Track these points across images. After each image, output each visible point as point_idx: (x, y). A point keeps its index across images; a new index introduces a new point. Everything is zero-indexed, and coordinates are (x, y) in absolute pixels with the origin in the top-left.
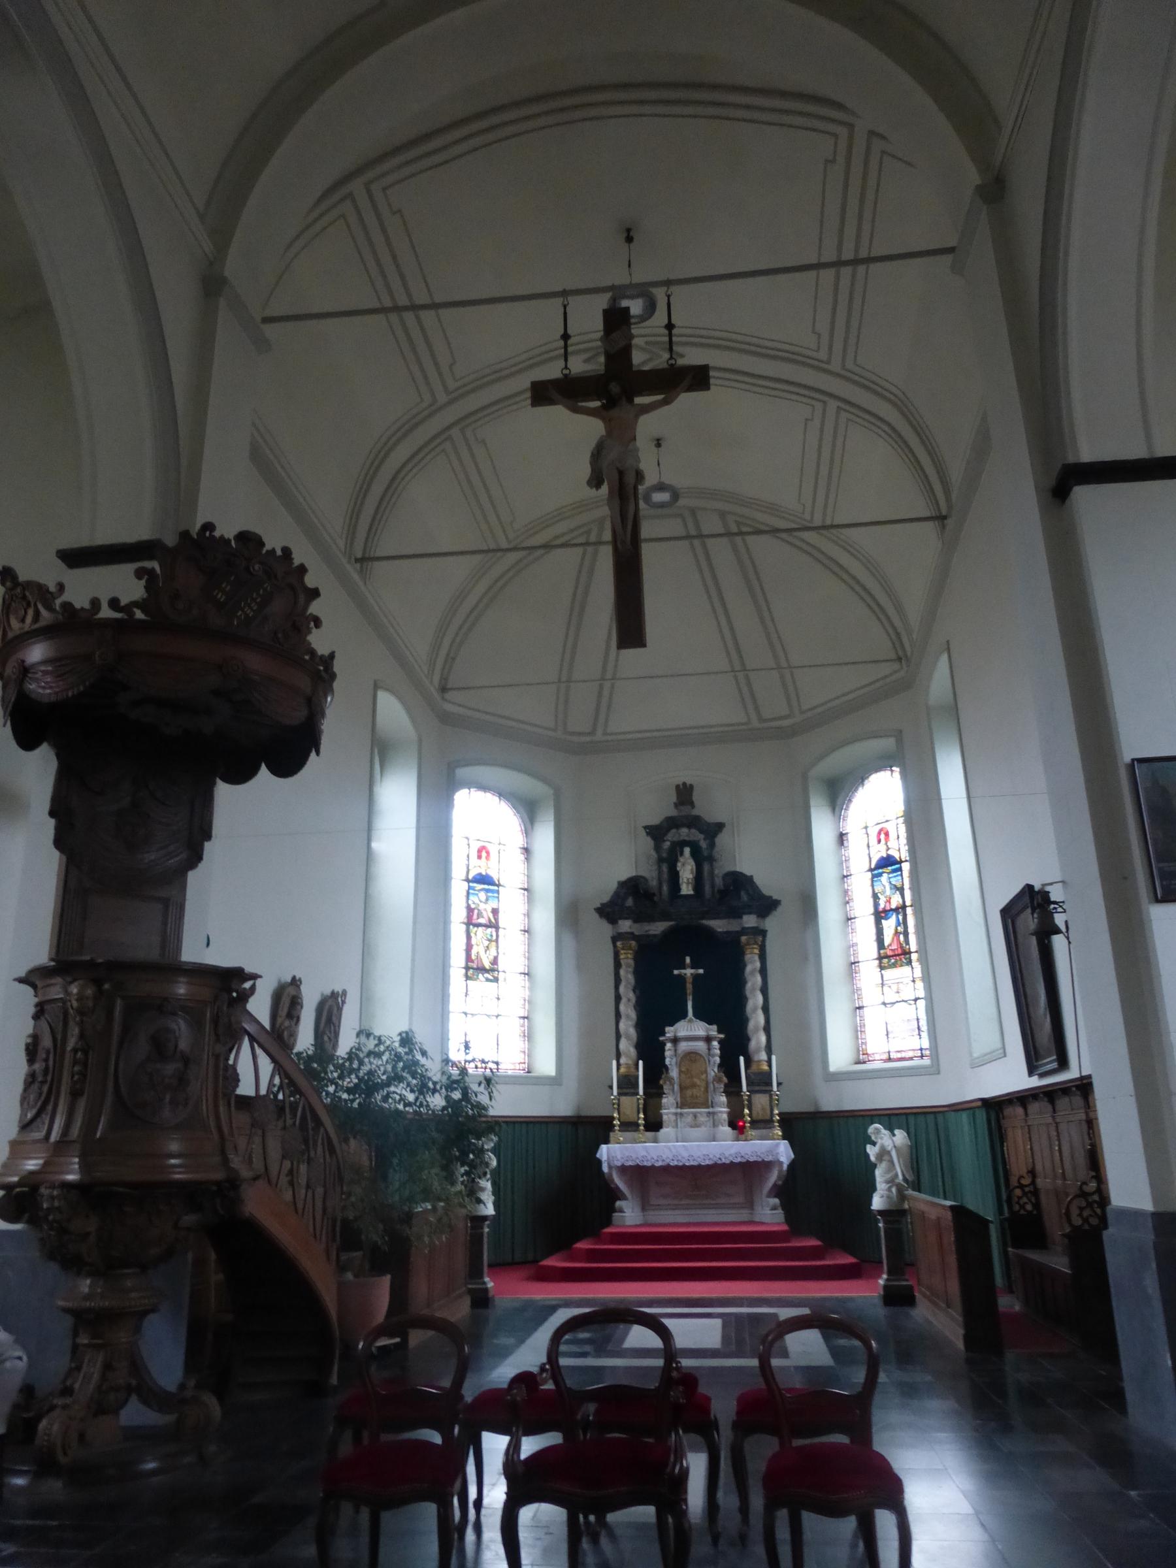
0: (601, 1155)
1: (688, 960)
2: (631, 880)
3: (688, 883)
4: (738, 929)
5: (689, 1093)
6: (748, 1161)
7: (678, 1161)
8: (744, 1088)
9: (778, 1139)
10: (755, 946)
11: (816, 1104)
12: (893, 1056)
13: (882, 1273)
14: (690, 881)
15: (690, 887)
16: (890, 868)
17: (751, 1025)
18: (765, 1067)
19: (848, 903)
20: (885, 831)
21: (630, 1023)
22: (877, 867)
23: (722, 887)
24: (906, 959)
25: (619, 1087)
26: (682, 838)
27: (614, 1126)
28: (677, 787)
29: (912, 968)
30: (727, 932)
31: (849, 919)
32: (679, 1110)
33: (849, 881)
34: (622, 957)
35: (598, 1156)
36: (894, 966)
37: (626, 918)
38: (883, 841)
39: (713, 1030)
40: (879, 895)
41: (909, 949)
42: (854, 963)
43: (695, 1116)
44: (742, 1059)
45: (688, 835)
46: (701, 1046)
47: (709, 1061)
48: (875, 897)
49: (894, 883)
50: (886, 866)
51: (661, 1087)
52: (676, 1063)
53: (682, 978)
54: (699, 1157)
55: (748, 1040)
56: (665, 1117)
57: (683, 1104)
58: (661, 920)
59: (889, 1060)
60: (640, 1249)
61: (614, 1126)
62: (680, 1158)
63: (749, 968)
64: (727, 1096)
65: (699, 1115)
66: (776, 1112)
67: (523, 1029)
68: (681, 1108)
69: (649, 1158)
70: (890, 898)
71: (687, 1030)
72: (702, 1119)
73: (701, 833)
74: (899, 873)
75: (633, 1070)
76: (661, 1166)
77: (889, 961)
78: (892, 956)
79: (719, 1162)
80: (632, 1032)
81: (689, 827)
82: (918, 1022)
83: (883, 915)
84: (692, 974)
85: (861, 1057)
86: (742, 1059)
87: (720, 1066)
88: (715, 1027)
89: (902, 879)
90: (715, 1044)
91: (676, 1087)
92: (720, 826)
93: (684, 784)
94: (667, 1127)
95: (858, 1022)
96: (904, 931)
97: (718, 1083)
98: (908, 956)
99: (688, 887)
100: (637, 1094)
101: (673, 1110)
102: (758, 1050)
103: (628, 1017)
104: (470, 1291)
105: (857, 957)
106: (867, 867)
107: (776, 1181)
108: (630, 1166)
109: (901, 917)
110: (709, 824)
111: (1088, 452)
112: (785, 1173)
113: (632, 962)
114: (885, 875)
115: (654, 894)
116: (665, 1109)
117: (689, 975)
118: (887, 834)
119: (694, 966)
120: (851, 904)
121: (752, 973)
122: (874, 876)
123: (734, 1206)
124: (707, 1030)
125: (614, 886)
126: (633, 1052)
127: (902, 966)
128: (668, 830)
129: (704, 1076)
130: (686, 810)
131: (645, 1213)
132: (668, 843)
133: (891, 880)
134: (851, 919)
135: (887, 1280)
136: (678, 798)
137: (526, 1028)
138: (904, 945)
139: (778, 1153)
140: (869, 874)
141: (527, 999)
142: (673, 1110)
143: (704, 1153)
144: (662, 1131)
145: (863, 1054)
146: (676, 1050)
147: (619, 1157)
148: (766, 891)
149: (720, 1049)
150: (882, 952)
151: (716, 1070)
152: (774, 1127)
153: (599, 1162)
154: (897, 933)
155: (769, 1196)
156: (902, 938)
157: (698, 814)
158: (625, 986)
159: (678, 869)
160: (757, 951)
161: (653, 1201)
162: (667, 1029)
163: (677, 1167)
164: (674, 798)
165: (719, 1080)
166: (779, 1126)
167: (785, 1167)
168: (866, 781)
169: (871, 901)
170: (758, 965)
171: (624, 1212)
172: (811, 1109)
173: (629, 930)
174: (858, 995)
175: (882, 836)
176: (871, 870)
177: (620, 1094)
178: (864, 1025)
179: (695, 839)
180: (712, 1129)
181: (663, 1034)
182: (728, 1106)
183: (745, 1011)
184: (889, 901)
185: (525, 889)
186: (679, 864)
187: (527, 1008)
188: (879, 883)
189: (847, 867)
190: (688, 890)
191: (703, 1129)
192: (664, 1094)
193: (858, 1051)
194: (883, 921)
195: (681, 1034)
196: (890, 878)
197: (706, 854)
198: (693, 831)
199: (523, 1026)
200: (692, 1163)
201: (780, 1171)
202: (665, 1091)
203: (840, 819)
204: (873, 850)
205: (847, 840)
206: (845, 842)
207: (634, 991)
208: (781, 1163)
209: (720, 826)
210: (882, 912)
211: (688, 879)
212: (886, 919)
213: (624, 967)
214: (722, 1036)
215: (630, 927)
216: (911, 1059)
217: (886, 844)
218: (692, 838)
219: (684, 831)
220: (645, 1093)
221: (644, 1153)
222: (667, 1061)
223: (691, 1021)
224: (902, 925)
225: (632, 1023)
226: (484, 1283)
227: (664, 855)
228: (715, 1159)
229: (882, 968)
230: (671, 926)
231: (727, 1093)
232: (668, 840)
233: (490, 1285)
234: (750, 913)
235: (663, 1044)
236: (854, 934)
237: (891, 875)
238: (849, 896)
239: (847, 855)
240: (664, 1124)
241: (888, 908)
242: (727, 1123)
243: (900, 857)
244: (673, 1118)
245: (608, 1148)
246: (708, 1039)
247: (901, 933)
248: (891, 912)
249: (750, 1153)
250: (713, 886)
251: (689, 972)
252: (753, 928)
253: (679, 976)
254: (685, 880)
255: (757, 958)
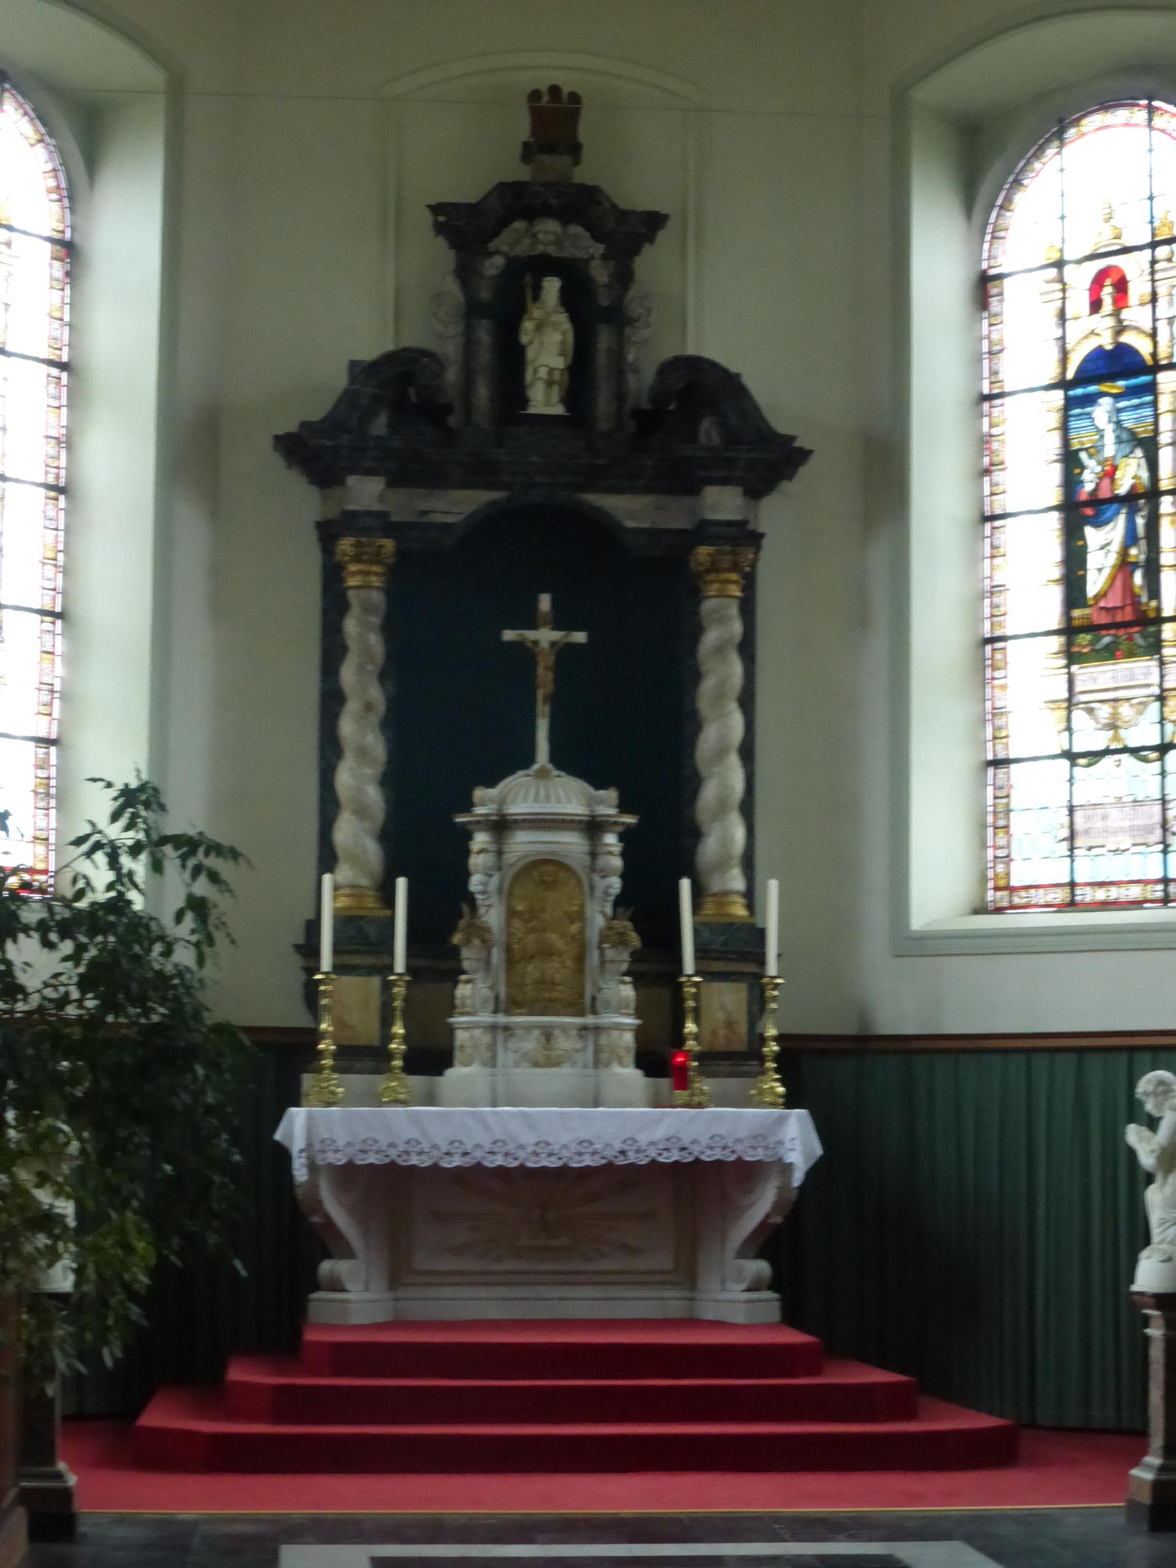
0: (290, 1134)
1: (545, 602)
2: (389, 359)
3: (550, 383)
4: (681, 523)
5: (532, 971)
6: (697, 1161)
7: (506, 1155)
8: (689, 964)
9: (773, 1105)
10: (734, 576)
11: (863, 1018)
12: (1086, 895)
13: (1144, 1451)
14: (557, 376)
15: (555, 394)
16: (1121, 383)
17: (708, 794)
18: (739, 910)
19: (987, 472)
21: (368, 771)
22: (1086, 375)
23: (646, 405)
24: (1145, 637)
25: (337, 951)
26: (540, 249)
27: (320, 1054)
28: (535, 95)
29: (1162, 663)
30: (654, 534)
32: (501, 1019)
33: (996, 412)
34: (352, 582)
35: (278, 1136)
36: (1110, 653)
37: (370, 472)
39: (607, 803)
40: (1083, 456)
41: (1158, 609)
43: (548, 1034)
44: (685, 885)
45: (558, 242)
46: (572, 843)
47: (592, 888)
48: (1070, 460)
49: (1127, 425)
50: (1112, 377)
51: (455, 953)
52: (500, 890)
53: (525, 654)
54: (565, 1146)
55: (696, 834)
56: (461, 1036)
57: (512, 1003)
58: (464, 484)
59: (1072, 905)
60: (418, 1387)
61: (320, 1054)
62: (511, 1147)
63: (711, 638)
64: (636, 985)
65: (557, 1032)
66: (772, 1032)
67: (42, 773)
68: (508, 1012)
69: (426, 1146)
70: (1115, 468)
71: (536, 800)
72: (564, 1044)
73: (595, 238)
74: (1149, 398)
75: (371, 903)
76: (458, 1168)
79: (620, 1161)
80: (374, 796)
81: (565, 217)
82: (1164, 810)
83: (1089, 511)
84: (553, 644)
85: (990, 895)
86: (685, 885)
87: (620, 902)
88: (611, 795)
89: (1156, 416)
90: (611, 839)
91: (497, 956)
92: (654, 222)
93: (555, 90)
94: (468, 1064)
95: (990, 801)
97: (614, 946)
98: (1152, 629)
99: (548, 395)
100: (390, 968)
101: (486, 1018)
102: (722, 865)
103: (363, 754)
104: (25, 1497)
105: (1001, 625)
106: (1051, 373)
107: (768, 1216)
108: (371, 1166)
109: (1140, 522)
110: (624, 216)
112: (793, 1196)
113: (377, 597)
114: (1106, 403)
115: (448, 409)
116: (463, 1014)
117: (545, 644)
118: (1121, 286)
119: (560, 622)
120: (998, 476)
121: (720, 650)
122: (1070, 403)
123: (642, 1279)
124: (591, 802)
125: (340, 380)
126: (373, 852)
127: (1131, 654)
128: (504, 223)
129: (574, 928)
130: (556, 163)
131: (400, 1293)
132: (498, 261)
134: (993, 518)
135: (1162, 1469)
136: (534, 133)
137: (53, 772)
138: (1144, 599)
139: (781, 1143)
140: (1058, 396)
141: (57, 687)
142: (486, 1018)
143: (583, 1135)
144: (450, 1073)
145: (996, 889)
146: (500, 853)
147: (341, 1143)
148: (780, 424)
149: (624, 855)
150: (1076, 613)
151: (609, 910)
152: (764, 1072)
153: (282, 1155)
154: (1125, 566)
155: (742, 1253)
156: (1138, 578)
157: (589, 182)
158: (361, 667)
159: (524, 339)
160: (735, 591)
161: (422, 1262)
162: (479, 793)
163: (501, 1171)
164: (522, 129)
165: (620, 941)
166: (777, 1071)
167: (798, 1178)
168: (1071, 132)
169: (1055, 473)
170: (737, 628)
171: (344, 1290)
172: (849, 1029)
173: (377, 507)
174: (996, 729)
175: (1107, 293)
176: (1062, 384)
177: (338, 969)
178: (1008, 811)
179: (579, 254)
180: (591, 1071)
181: (467, 805)
182: (638, 1014)
183: (692, 756)
184: (1110, 474)
185: (63, 366)
186: (528, 325)
187: (56, 714)
188: (1086, 423)
189: (994, 373)
190: (548, 403)
191: (565, 1070)
192: (464, 972)
193: (984, 879)
194: (1089, 531)
195: (518, 808)
196: (1119, 411)
197: (605, 302)
198: (575, 229)
199: (42, 765)
200: (545, 1162)
201: (783, 1189)
202: (466, 965)
203: (984, 234)
204: (1074, 331)
205: (1001, 294)
206: (994, 301)
207: (382, 677)
208: (787, 1169)
209: (654, 222)
210: (1087, 504)
211: (551, 371)
212: (1098, 524)
213: (355, 609)
214: (630, 820)
215: (381, 498)
216: (1137, 904)
217: (1116, 313)
218: (568, 252)
219: (549, 228)
220: (410, 969)
221: (412, 1132)
222: (475, 883)
223: (542, 774)
224: (1143, 543)
225: (373, 771)
226: (59, 1476)
227: (485, 295)
228: (610, 1153)
229: (1072, 656)
230: (494, 503)
231: (638, 978)
232: (498, 252)
233: (72, 1480)
234: (725, 482)
235: (466, 834)
236: (997, 561)
237: (1122, 404)
238: (992, 452)
239: (994, 336)
240: (458, 1055)
241: (1104, 494)
242: (630, 1058)
243: (1154, 355)
244: (485, 1038)
245: (310, 1118)
246: (593, 827)
247: (1136, 565)
248: (1115, 506)
249: (705, 1141)
250: (620, 396)
251: (546, 636)
252: (730, 523)
253: (519, 645)
254: (543, 373)
255: (733, 609)
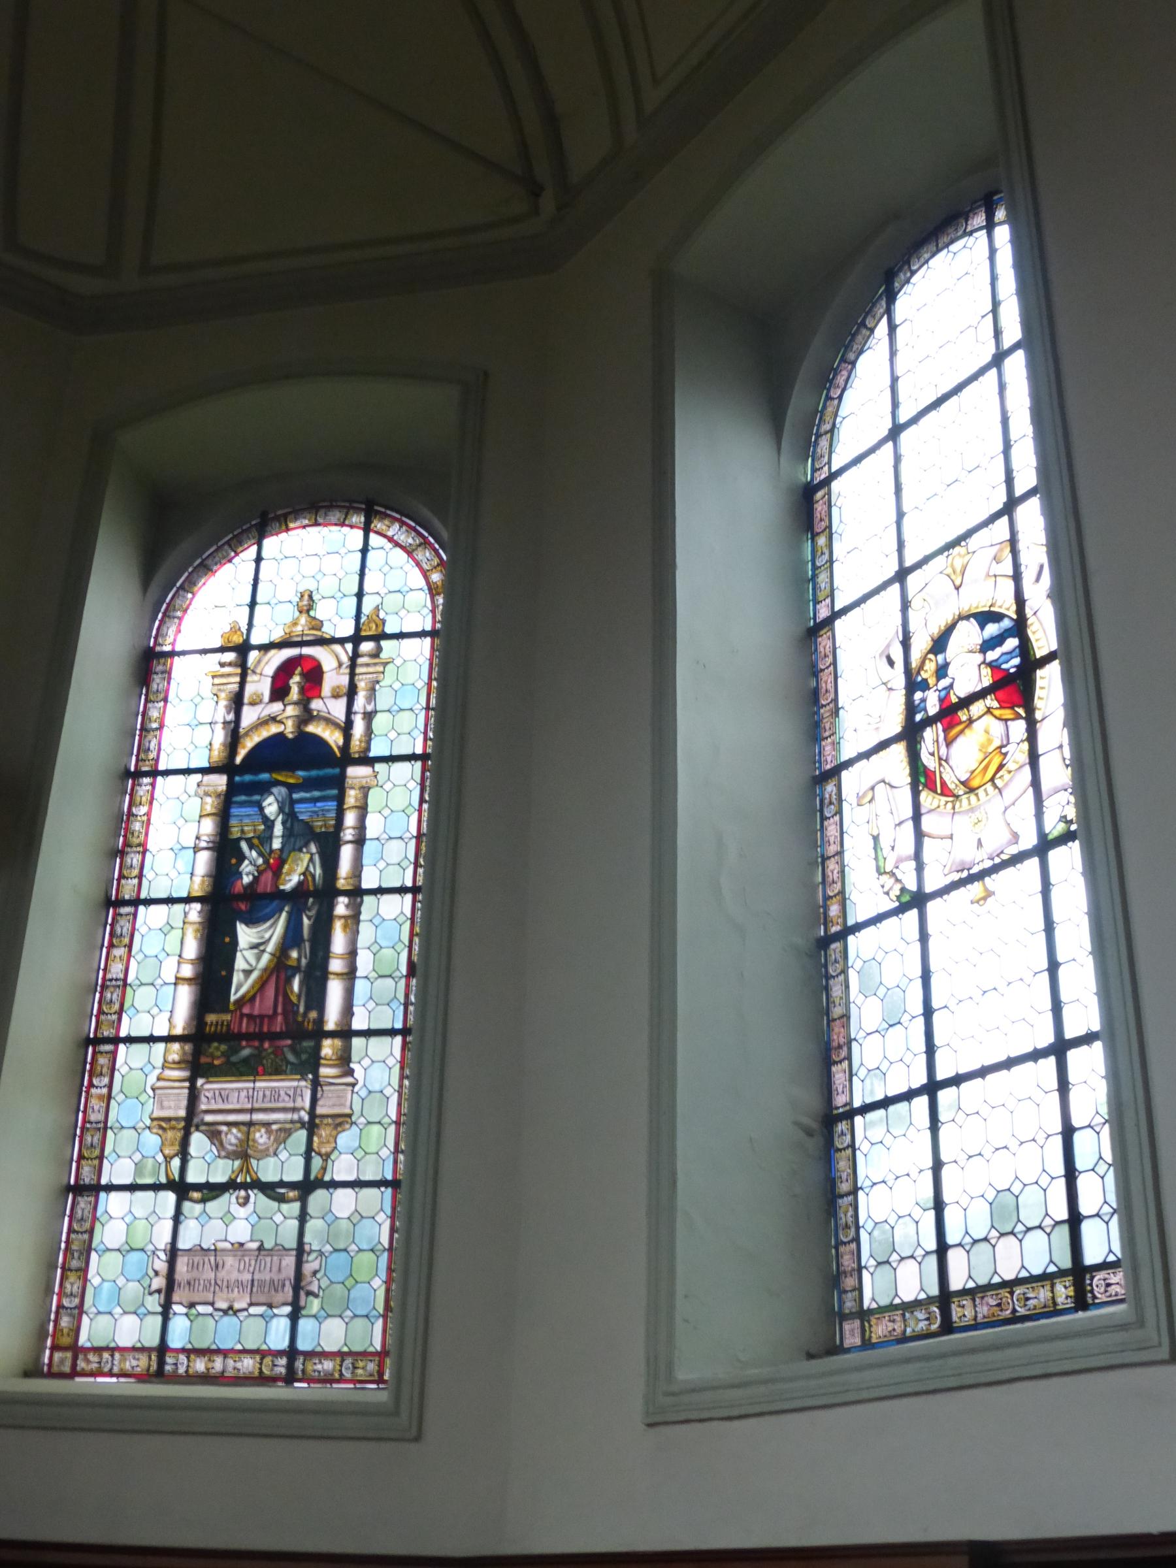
20: (309, 666)
31: (113, 903)
38: (294, 694)
42: (97, 1041)
50: (290, 766)
59: (159, 1375)
74: (335, 792)
77: (235, 1050)
78: (249, 1037)
96: (310, 965)
98: (308, 1044)
111: (329, 1282)
122: (232, 789)
133: (299, 808)
154: (280, 969)
193: (42, 1334)
247: (297, 969)
